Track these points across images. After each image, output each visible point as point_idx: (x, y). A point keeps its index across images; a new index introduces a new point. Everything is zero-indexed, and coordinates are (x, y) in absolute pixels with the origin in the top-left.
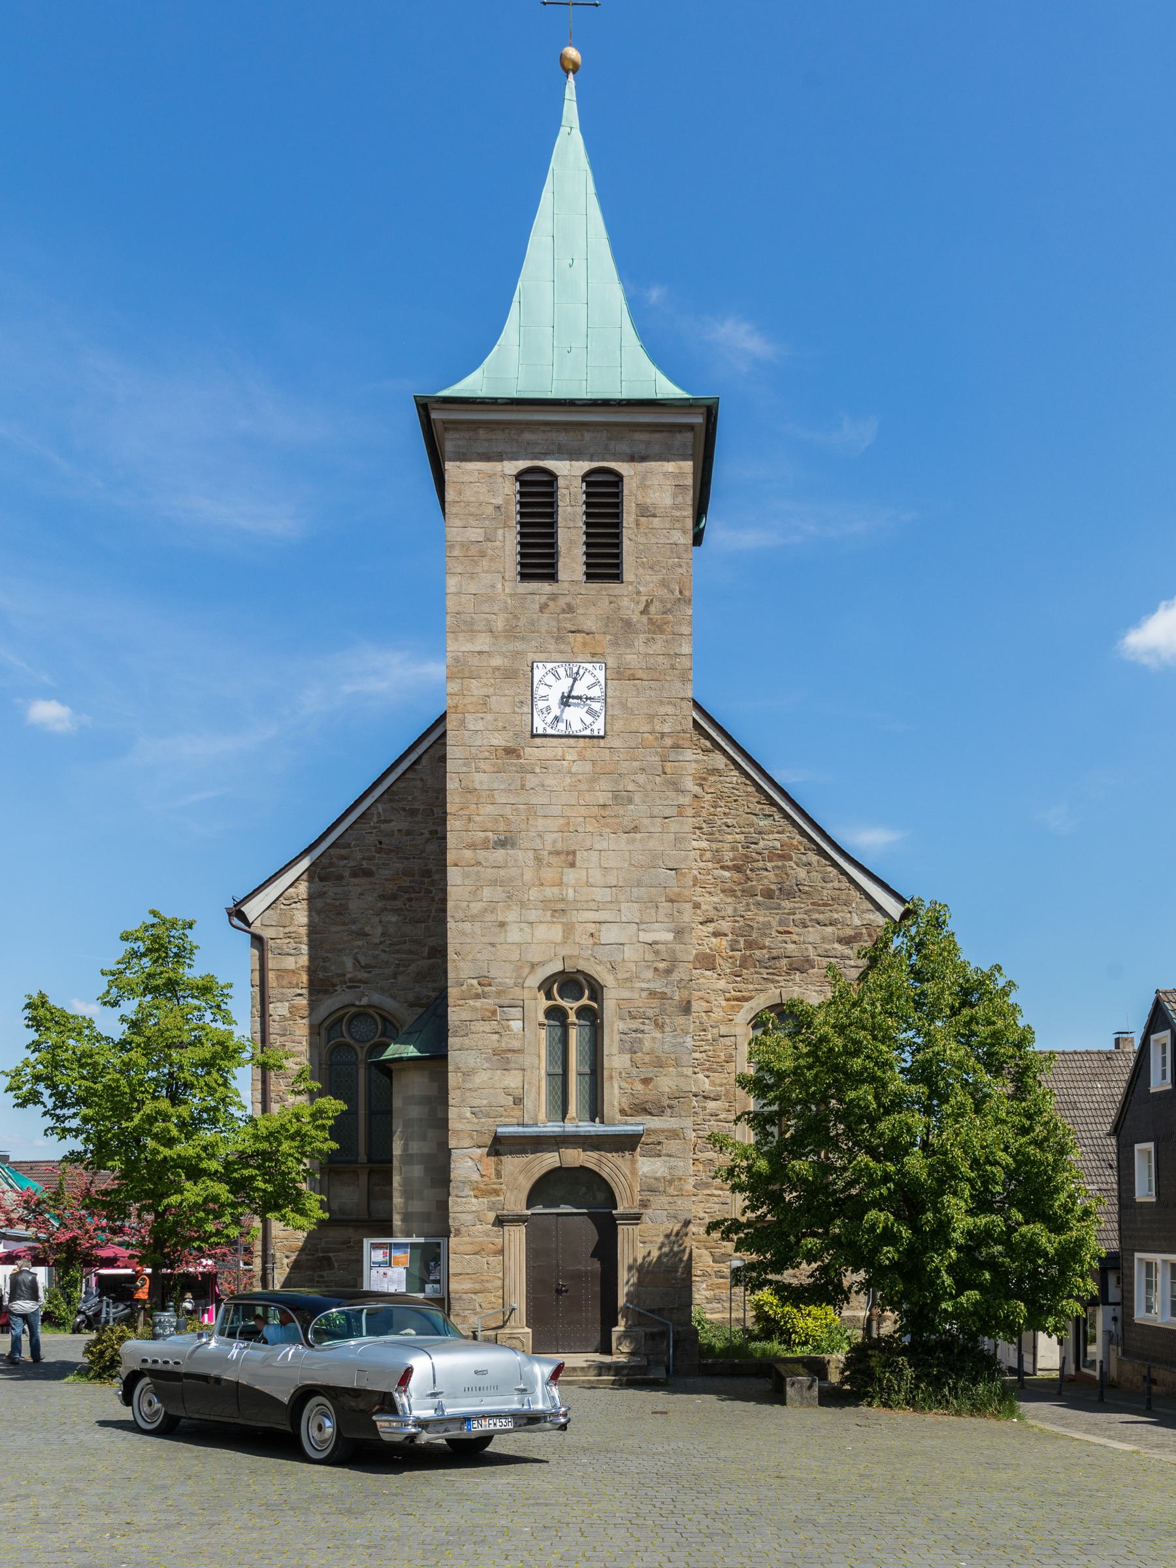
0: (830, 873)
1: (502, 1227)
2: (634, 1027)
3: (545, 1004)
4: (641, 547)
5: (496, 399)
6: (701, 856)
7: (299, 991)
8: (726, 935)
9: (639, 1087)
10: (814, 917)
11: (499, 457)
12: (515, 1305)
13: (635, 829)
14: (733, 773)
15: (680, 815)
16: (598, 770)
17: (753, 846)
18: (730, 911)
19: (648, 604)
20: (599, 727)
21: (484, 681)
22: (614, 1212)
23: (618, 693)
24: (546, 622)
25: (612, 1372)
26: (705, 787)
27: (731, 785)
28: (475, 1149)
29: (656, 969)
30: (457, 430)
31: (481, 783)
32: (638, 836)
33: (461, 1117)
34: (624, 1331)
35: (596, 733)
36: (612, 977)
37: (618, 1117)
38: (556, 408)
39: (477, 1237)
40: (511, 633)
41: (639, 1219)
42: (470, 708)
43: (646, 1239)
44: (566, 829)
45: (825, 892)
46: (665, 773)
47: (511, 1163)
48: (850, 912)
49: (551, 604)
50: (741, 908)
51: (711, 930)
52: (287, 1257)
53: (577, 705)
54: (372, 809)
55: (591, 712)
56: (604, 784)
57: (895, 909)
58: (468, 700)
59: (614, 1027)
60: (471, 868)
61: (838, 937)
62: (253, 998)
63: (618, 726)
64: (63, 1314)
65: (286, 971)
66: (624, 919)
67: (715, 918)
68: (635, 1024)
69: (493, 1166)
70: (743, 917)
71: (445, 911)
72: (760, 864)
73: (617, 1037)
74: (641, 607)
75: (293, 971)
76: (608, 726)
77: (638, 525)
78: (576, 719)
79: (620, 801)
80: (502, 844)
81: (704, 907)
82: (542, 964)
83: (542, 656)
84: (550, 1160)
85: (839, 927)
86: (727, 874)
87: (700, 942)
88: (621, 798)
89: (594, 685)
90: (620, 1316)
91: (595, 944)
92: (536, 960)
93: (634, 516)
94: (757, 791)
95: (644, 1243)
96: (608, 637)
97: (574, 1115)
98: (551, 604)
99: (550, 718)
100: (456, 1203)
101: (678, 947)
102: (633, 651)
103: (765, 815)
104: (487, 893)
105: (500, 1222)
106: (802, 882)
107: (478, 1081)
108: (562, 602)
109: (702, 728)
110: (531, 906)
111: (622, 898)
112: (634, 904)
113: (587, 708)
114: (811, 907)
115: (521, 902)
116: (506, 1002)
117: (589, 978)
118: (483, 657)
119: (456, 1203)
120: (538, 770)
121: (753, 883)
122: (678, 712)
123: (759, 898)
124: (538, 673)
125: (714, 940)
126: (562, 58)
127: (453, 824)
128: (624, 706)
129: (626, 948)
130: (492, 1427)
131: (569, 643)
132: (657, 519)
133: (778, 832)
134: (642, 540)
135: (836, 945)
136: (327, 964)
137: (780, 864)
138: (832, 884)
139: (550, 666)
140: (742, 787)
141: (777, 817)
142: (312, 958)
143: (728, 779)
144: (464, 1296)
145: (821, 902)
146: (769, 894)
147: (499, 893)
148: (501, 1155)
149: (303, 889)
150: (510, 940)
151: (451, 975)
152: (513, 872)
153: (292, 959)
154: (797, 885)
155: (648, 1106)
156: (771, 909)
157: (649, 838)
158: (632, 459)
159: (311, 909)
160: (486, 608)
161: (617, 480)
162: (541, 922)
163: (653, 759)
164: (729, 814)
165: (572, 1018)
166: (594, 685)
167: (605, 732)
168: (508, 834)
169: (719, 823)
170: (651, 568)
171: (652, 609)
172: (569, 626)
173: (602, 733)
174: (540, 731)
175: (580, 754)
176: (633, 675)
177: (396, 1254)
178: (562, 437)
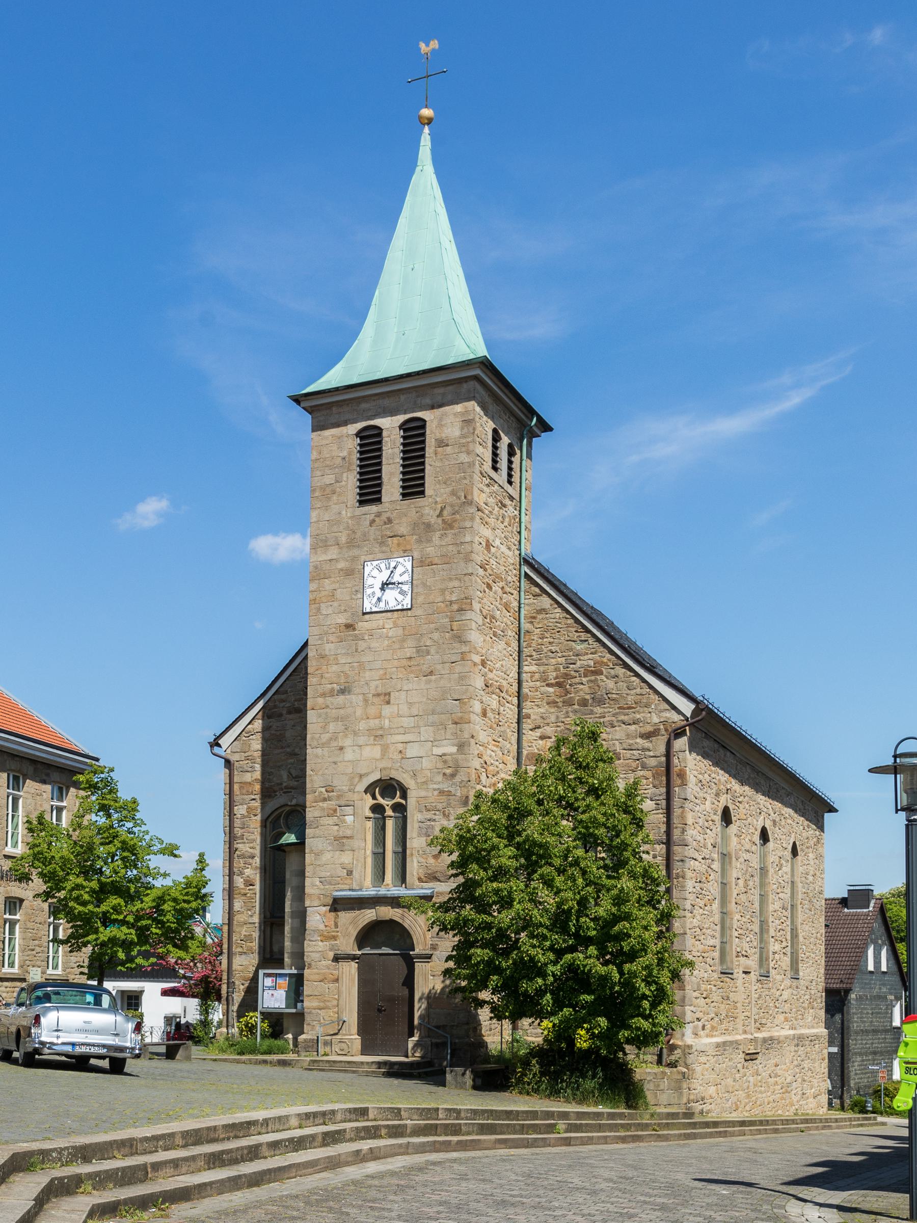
0: (633, 682)
1: (338, 962)
2: (428, 817)
3: (370, 802)
4: (438, 469)
5: (338, 388)
6: (532, 677)
7: (253, 797)
8: (550, 738)
9: (431, 861)
10: (620, 719)
11: (345, 423)
12: (345, 1019)
13: (431, 673)
14: (556, 611)
15: (463, 659)
16: (406, 632)
17: (571, 666)
18: (553, 719)
19: (442, 510)
20: (407, 603)
21: (332, 579)
22: (411, 953)
23: (420, 576)
24: (373, 532)
25: (387, 1067)
26: (534, 623)
27: (554, 620)
28: (322, 907)
29: (444, 774)
30: (319, 410)
31: (330, 650)
32: (433, 677)
33: (313, 885)
34: (417, 1041)
35: (405, 607)
36: (414, 782)
37: (417, 883)
38: (378, 385)
39: (321, 969)
40: (352, 543)
41: (430, 958)
42: (324, 600)
43: (435, 973)
44: (384, 677)
45: (629, 698)
46: (452, 630)
47: (345, 917)
48: (650, 713)
49: (377, 519)
50: (562, 715)
51: (538, 734)
52: (243, 984)
53: (391, 589)
54: (302, 664)
55: (402, 593)
56: (410, 643)
57: (687, 707)
58: (323, 593)
59: (414, 817)
60: (322, 711)
61: (640, 733)
62: (225, 803)
63: (420, 599)
64: (199, 1034)
65: (246, 783)
66: (423, 739)
67: (542, 725)
68: (429, 815)
69: (333, 919)
70: (563, 722)
71: (305, 739)
72: (577, 680)
73: (416, 825)
74: (438, 512)
75: (250, 783)
76: (414, 600)
77: (436, 454)
78: (392, 598)
79: (421, 654)
80: (342, 692)
81: (533, 717)
82: (367, 774)
83: (371, 557)
84: (369, 915)
85: (641, 725)
86: (551, 690)
87: (530, 744)
88: (422, 651)
89: (404, 573)
90: (416, 1031)
91: (403, 758)
92: (363, 772)
93: (433, 448)
94: (575, 622)
95: (433, 976)
96: (415, 537)
97: (390, 882)
98: (377, 519)
99: (375, 599)
100: (309, 945)
101: (460, 757)
102: (432, 545)
103: (581, 641)
104: (332, 727)
105: (336, 959)
106: (611, 691)
107: (324, 859)
108: (384, 517)
109: (532, 578)
110: (361, 734)
111: (421, 724)
112: (430, 728)
113: (399, 590)
114: (618, 711)
115: (354, 731)
116: (343, 803)
117: (398, 782)
118: (333, 563)
119: (309, 945)
120: (366, 638)
121: (572, 695)
122: (462, 585)
123: (576, 707)
124: (367, 570)
125: (540, 742)
126: (420, 118)
127: (311, 680)
128: (424, 585)
129: (424, 760)
130: (88, 1050)
131: (389, 545)
132: (449, 447)
133: (592, 653)
134: (438, 464)
135: (639, 740)
136: (271, 777)
137: (593, 678)
138: (635, 691)
139: (375, 563)
140: (563, 621)
141: (590, 642)
142: (263, 773)
143: (552, 616)
144: (313, 1011)
145: (626, 706)
146: (584, 703)
147: (340, 726)
148: (338, 911)
149: (258, 725)
150: (346, 759)
151: (308, 785)
152: (349, 711)
153: (249, 774)
154: (607, 694)
155: (438, 875)
156: (586, 715)
157: (440, 678)
158: (433, 407)
159: (265, 740)
160: (335, 529)
161: (421, 424)
162: (367, 745)
163: (445, 620)
164: (553, 643)
165: (389, 812)
166: (404, 573)
167: (412, 605)
168: (347, 685)
169: (545, 650)
170: (445, 483)
171: (445, 513)
172: (389, 533)
173: (409, 607)
174: (368, 610)
175: (394, 623)
176: (431, 562)
177: (280, 981)
178: (386, 402)
